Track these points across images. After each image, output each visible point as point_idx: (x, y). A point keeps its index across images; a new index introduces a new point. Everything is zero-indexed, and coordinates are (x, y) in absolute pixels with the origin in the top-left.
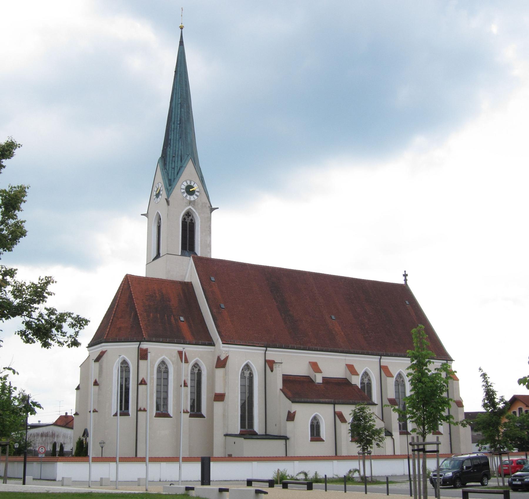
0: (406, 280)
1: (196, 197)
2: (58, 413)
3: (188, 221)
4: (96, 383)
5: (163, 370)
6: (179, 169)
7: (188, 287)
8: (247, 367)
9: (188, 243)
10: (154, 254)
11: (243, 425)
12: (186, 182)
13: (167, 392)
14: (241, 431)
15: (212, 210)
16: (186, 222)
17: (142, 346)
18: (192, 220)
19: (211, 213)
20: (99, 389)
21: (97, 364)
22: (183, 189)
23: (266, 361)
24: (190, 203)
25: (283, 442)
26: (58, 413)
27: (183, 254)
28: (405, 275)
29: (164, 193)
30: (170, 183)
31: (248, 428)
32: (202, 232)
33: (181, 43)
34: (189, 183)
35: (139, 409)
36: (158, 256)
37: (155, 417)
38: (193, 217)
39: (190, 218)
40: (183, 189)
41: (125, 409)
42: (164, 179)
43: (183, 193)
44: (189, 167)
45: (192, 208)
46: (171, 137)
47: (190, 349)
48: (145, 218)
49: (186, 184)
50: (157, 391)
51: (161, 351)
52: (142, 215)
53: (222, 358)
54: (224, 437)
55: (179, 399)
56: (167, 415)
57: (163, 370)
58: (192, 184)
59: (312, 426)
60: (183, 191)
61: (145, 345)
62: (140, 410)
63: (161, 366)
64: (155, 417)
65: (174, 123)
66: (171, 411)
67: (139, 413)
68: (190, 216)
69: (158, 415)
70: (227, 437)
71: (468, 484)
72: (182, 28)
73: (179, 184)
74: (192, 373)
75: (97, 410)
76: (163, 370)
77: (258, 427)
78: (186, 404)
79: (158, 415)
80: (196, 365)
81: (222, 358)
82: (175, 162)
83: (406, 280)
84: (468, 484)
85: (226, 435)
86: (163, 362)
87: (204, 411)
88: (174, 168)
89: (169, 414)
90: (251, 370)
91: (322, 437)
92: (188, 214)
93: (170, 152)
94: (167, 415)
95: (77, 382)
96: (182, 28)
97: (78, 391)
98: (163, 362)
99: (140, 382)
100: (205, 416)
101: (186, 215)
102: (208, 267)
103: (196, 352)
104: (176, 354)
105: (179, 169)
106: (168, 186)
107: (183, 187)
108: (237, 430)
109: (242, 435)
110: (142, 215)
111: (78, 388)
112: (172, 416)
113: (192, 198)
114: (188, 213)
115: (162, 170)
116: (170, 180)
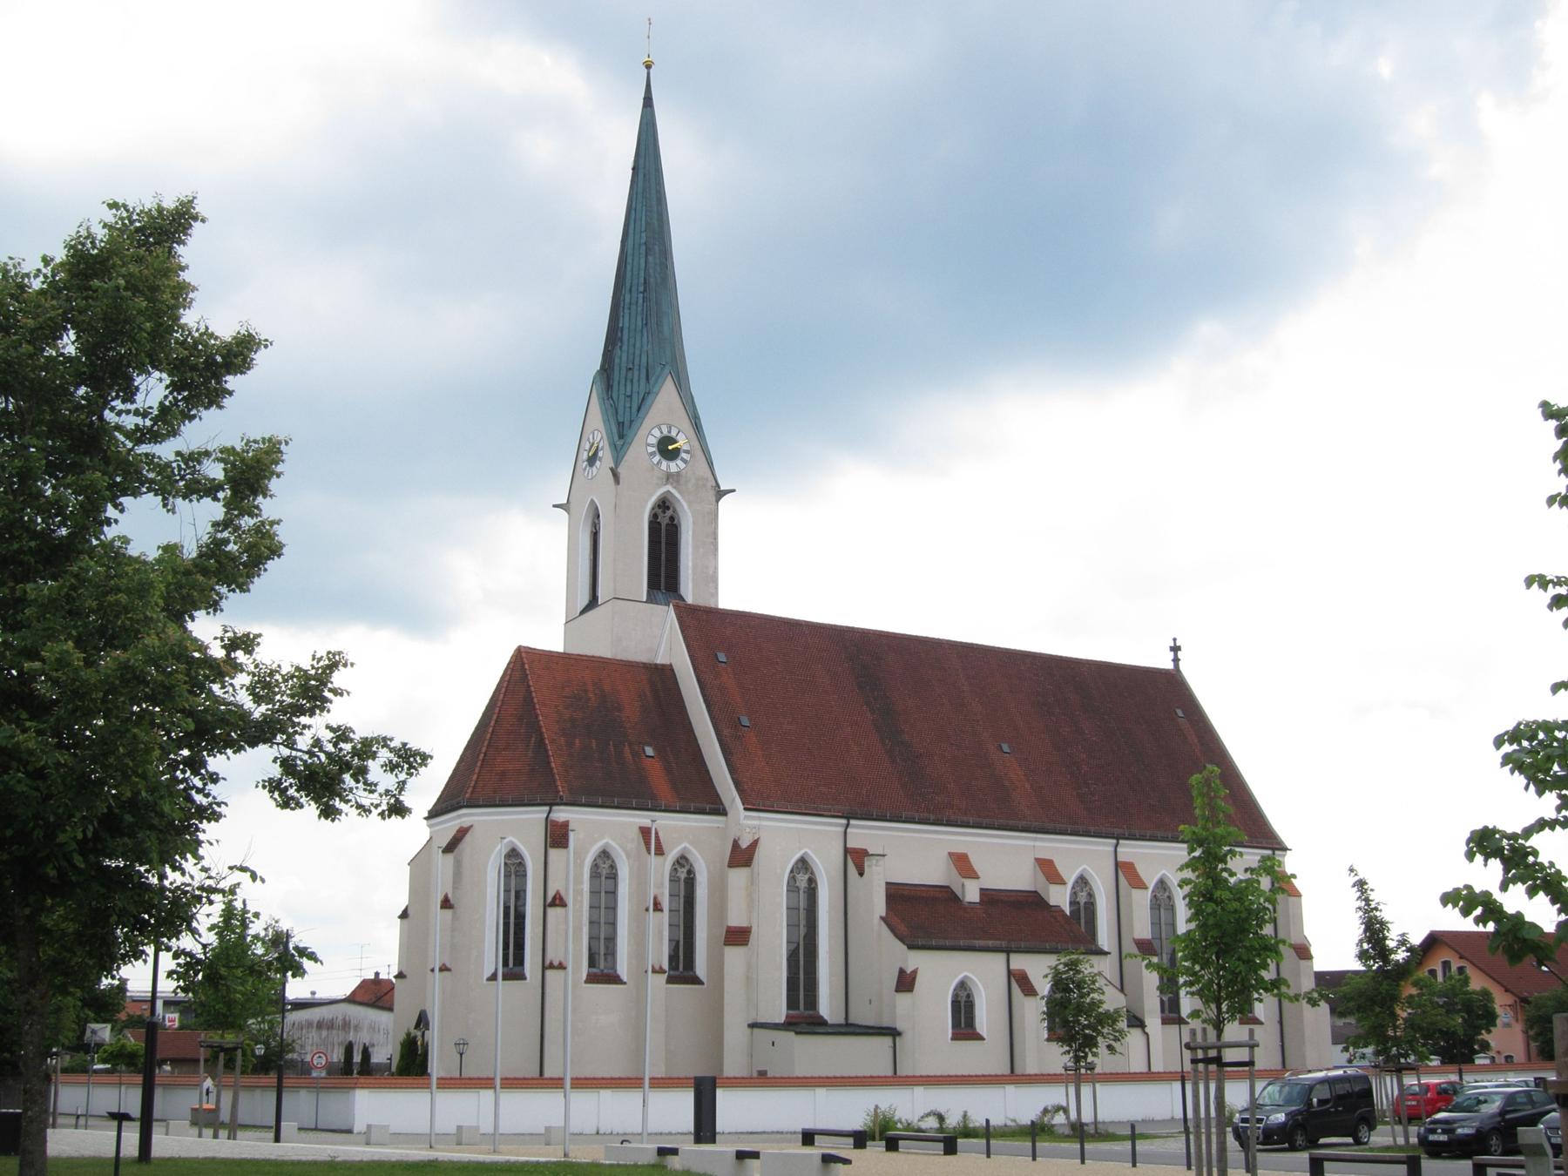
0: (1176, 660)
1: (682, 465)
3: (664, 521)
4: (446, 904)
5: (604, 871)
7: (663, 677)
8: (803, 864)
10: (584, 599)
11: (792, 1003)
15: (720, 494)
18: (672, 518)
21: (450, 857)
23: (847, 851)
24: (669, 477)
25: (888, 1041)
27: (651, 599)
28: (1175, 649)
29: (606, 456)
30: (622, 431)
32: (695, 547)
33: (648, 102)
36: (593, 603)
42: (606, 422)
43: (653, 454)
44: (666, 397)
46: (624, 322)
47: (668, 824)
50: (591, 923)
51: (601, 828)
53: (744, 844)
54: (748, 1031)
55: (642, 940)
56: (614, 979)
57: (604, 871)
59: (956, 1003)
60: (651, 450)
61: (562, 814)
62: (551, 966)
63: (600, 862)
66: (623, 969)
71: (1322, 1141)
72: (648, 67)
73: (642, 432)
74: (674, 879)
77: (827, 1006)
79: (592, 979)
80: (682, 861)
81: (744, 844)
83: (1176, 660)
84: (1322, 1141)
86: (605, 854)
87: (701, 969)
91: (979, 1030)
92: (664, 504)
93: (621, 357)
94: (614, 979)
96: (648, 67)
98: (605, 854)
99: (549, 899)
102: (712, 630)
103: (683, 831)
104: (635, 835)
107: (653, 440)
108: (780, 1013)
109: (790, 1025)
111: (404, 915)
113: (673, 466)
115: (602, 401)
116: (620, 425)
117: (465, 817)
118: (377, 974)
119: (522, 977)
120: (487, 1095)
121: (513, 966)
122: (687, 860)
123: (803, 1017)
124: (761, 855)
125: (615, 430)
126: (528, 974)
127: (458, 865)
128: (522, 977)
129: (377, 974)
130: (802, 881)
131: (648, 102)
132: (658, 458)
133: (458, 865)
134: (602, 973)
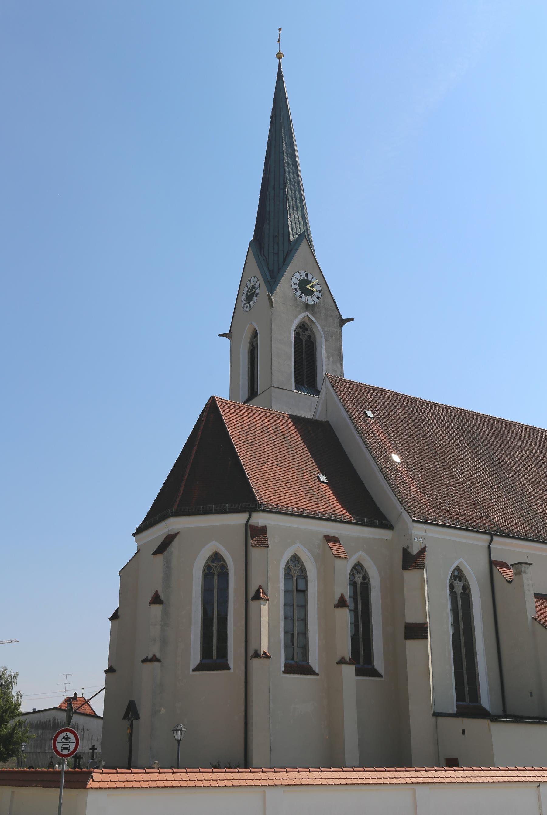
1: (316, 300)
2: (64, 693)
4: (156, 600)
6: (287, 255)
9: (306, 374)
11: (460, 696)
12: (300, 274)
13: (305, 620)
14: (458, 707)
15: (343, 322)
16: (301, 339)
17: (253, 522)
18: (309, 337)
19: (341, 327)
20: (166, 613)
21: (160, 558)
22: (295, 284)
24: (307, 306)
26: (64, 693)
29: (262, 289)
31: (470, 701)
32: (328, 358)
33: (280, 77)
34: (304, 276)
35: (251, 652)
37: (284, 672)
38: (312, 331)
39: (307, 333)
40: (295, 284)
41: (218, 657)
42: (261, 268)
43: (296, 290)
45: (311, 316)
48: (227, 342)
49: (299, 277)
50: (286, 618)
52: (220, 335)
53: (415, 551)
54: (433, 719)
55: (328, 632)
56: (308, 671)
57: (295, 571)
58: (309, 277)
60: (294, 287)
62: (257, 655)
63: (292, 565)
64: (284, 672)
65: (274, 188)
66: (314, 661)
67: (255, 663)
68: (307, 330)
69: (289, 669)
70: (440, 719)
73: (287, 275)
75: (158, 656)
76: (295, 572)
77: (486, 700)
78: (345, 649)
79: (289, 669)
81: (415, 551)
82: (278, 244)
85: (436, 715)
86: (295, 559)
87: (379, 663)
88: (278, 253)
89: (311, 668)
90: (466, 581)
92: (303, 327)
94: (308, 671)
95: (115, 605)
97: (116, 622)
98: (295, 559)
99: (252, 594)
100: (383, 674)
101: (300, 327)
105: (287, 255)
106: (269, 278)
107: (295, 280)
109: (462, 713)
110: (220, 335)
111: (115, 617)
112: (317, 671)
114: (303, 325)
116: (271, 272)
117: (175, 524)
118: (75, 694)
119: (226, 667)
120: (52, 794)
121: (213, 656)
122: (362, 566)
123: (468, 705)
124: (428, 558)
125: (267, 273)
126: (231, 665)
127: (168, 566)
128: (226, 667)
129: (75, 694)
130: (458, 586)
131: (280, 77)
132: (298, 293)
133: (168, 566)
134: (297, 665)
